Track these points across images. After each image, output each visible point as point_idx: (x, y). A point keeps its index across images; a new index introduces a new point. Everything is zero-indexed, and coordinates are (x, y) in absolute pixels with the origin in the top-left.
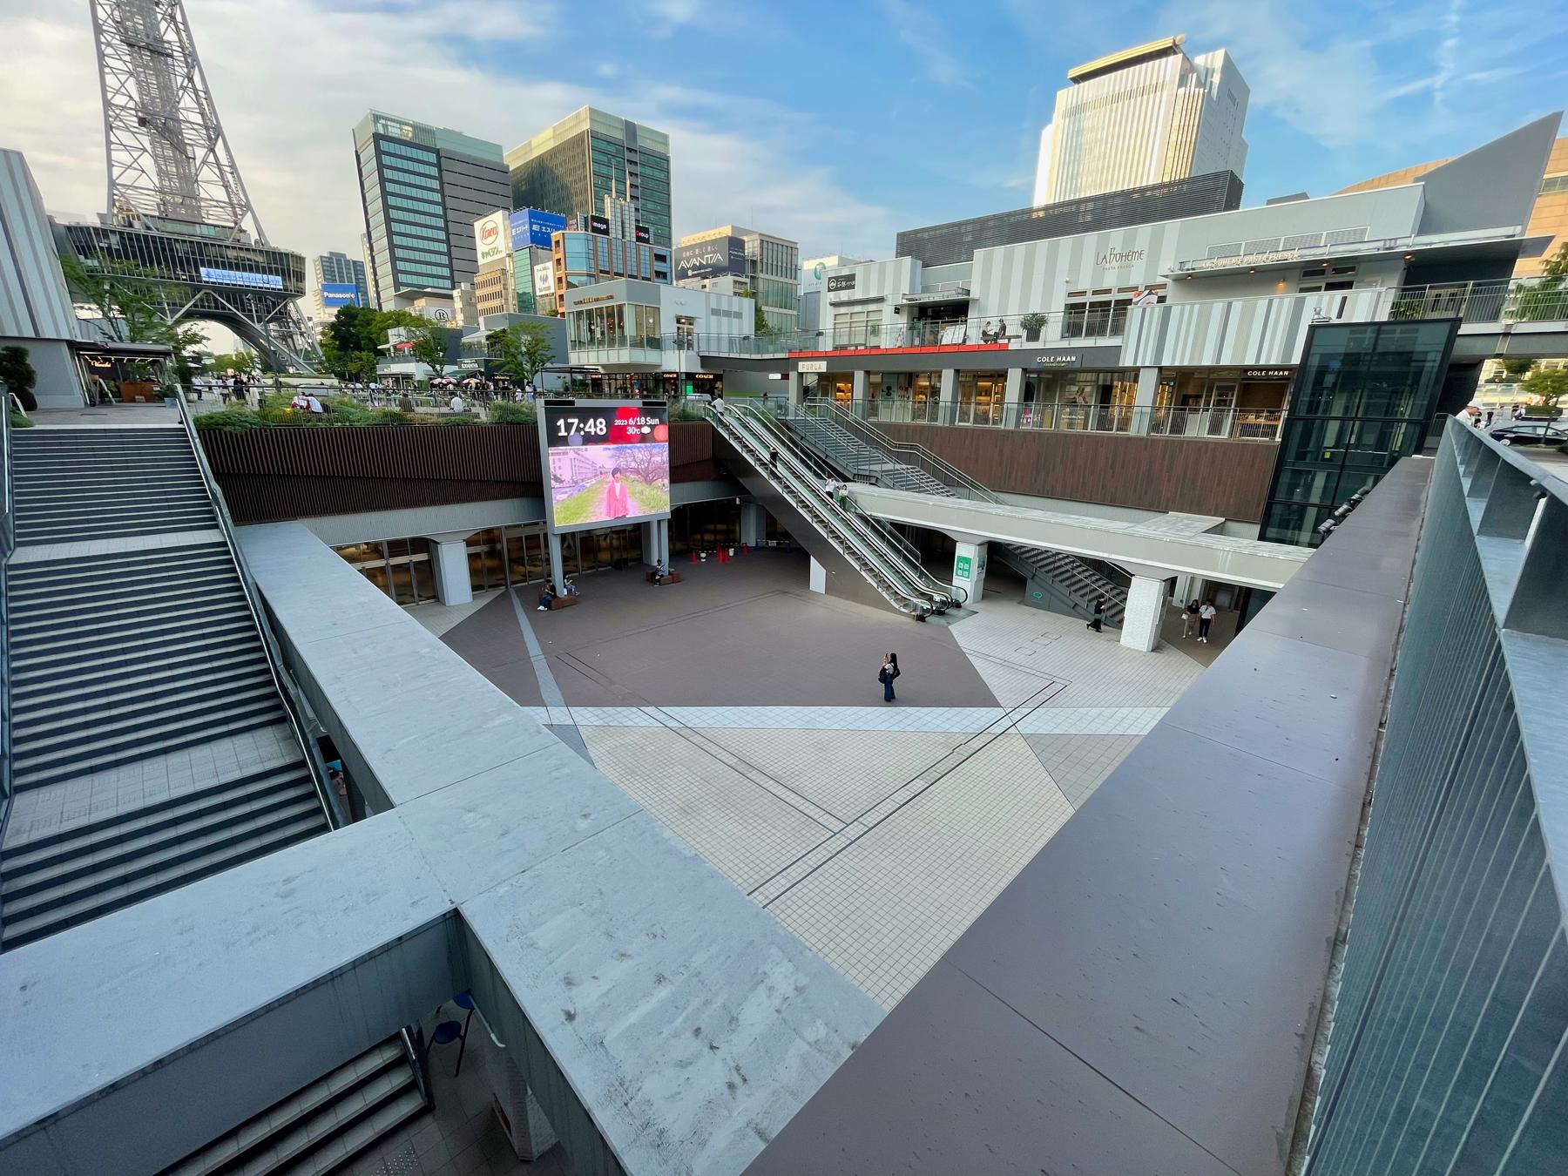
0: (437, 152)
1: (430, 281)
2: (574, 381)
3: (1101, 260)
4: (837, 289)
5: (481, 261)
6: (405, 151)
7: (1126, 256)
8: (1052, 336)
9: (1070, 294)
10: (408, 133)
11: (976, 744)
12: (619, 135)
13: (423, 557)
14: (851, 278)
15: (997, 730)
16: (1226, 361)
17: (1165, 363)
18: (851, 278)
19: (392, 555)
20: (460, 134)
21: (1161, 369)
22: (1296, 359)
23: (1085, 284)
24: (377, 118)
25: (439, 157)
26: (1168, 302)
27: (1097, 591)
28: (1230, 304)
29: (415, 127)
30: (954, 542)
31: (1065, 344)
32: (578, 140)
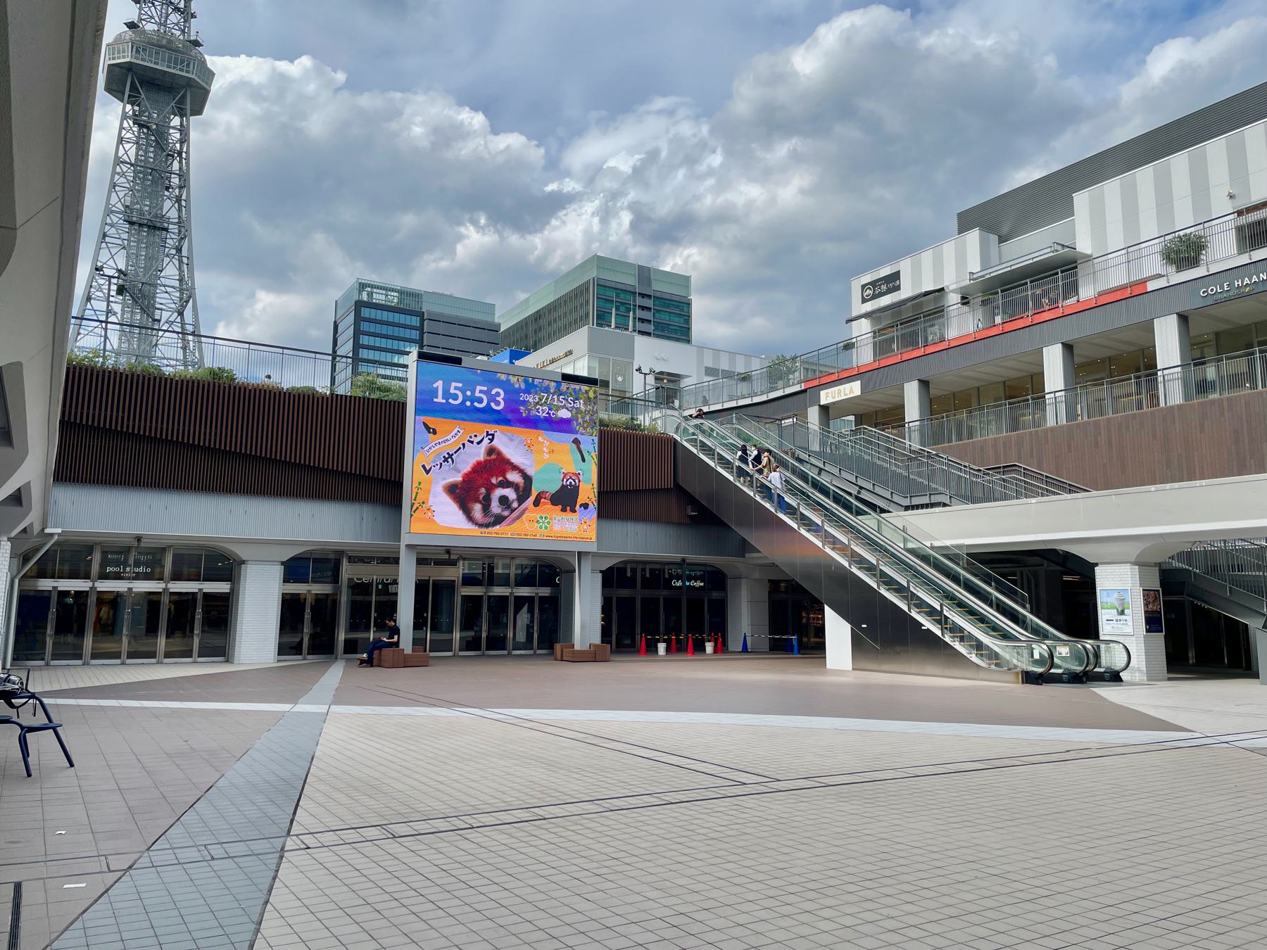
0: (421, 315)
4: (874, 297)
6: (385, 316)
8: (1224, 252)
10: (394, 299)
12: (630, 280)
14: (896, 276)
18: (896, 276)
19: (176, 577)
24: (362, 286)
25: (422, 320)
31: (1244, 259)
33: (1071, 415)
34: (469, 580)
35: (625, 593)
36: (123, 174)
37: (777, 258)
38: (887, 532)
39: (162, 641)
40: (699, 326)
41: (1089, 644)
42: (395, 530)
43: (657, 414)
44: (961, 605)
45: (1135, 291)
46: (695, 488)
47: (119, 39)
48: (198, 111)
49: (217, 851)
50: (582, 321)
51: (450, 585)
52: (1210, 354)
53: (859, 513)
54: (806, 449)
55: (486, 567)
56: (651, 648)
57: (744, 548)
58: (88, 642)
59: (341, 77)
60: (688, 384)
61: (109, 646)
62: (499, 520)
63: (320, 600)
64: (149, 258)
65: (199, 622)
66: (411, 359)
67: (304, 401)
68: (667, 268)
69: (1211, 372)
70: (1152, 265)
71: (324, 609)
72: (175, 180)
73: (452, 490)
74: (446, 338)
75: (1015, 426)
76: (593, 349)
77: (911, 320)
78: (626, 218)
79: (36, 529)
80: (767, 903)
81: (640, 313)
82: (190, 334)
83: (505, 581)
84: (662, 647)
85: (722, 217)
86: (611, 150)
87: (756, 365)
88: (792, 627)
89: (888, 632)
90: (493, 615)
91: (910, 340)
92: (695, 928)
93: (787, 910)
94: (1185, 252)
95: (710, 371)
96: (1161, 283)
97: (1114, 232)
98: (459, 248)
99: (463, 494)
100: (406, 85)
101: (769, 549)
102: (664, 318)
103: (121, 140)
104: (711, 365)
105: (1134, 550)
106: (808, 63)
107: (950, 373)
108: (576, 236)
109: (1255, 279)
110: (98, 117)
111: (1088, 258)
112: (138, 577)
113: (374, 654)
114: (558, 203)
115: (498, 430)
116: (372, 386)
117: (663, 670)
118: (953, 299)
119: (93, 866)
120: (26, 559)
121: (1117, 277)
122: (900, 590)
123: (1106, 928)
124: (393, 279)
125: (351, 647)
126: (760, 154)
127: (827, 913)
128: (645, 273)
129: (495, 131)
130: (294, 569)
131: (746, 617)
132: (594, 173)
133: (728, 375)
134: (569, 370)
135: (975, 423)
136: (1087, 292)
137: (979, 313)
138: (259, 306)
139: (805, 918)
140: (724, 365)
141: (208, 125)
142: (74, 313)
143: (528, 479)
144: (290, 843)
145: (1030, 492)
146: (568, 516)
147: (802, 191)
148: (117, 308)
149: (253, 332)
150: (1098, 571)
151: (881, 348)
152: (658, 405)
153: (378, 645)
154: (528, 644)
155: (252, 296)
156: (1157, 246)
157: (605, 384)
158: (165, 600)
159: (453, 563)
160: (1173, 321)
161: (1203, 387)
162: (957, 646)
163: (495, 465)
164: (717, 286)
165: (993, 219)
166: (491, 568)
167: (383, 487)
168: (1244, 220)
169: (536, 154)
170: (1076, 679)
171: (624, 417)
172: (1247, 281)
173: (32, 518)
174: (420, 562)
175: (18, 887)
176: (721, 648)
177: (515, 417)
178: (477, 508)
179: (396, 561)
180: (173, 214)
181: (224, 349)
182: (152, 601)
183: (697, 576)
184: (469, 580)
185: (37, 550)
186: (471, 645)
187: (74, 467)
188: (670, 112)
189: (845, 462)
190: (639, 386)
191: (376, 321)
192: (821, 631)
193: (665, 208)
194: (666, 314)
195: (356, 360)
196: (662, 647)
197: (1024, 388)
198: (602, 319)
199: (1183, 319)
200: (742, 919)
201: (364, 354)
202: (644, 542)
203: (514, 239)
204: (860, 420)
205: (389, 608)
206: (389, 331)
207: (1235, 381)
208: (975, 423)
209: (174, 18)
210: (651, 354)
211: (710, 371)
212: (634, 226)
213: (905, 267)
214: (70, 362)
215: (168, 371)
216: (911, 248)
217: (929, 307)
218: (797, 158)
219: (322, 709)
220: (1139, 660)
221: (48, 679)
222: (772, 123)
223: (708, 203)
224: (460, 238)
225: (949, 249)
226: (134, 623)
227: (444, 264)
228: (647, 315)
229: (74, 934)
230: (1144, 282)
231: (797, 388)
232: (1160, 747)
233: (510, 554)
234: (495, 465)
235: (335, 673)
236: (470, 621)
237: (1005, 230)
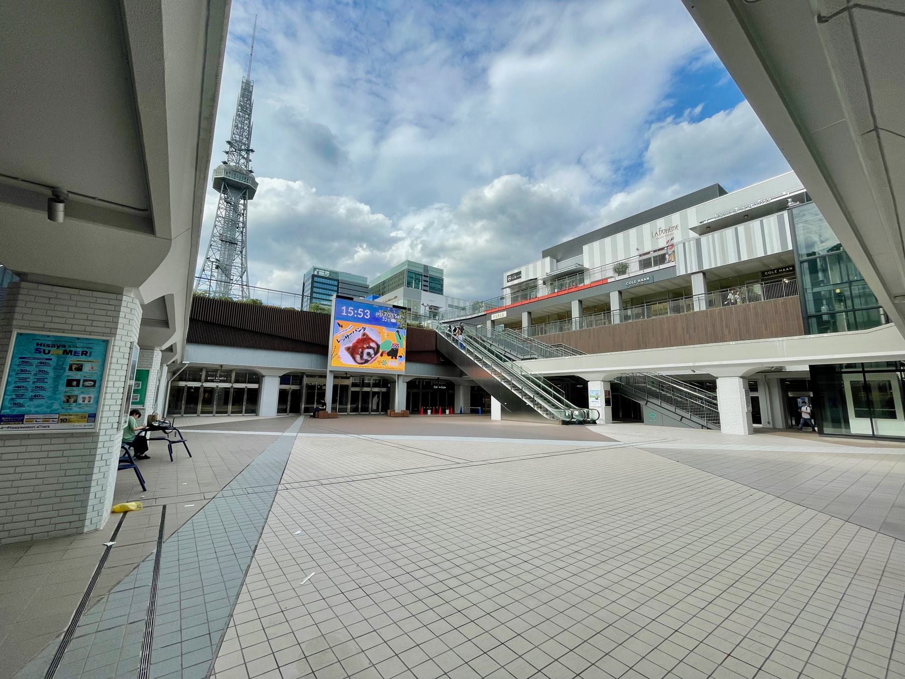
0: (338, 281)
3: (654, 235)
7: (669, 230)
8: (634, 269)
10: (327, 274)
12: (421, 271)
14: (520, 273)
16: (744, 258)
17: (706, 267)
18: (520, 273)
19: (237, 381)
20: (350, 274)
21: (704, 273)
22: (790, 248)
23: (648, 247)
24: (315, 269)
27: (695, 398)
28: (736, 229)
29: (330, 272)
30: (585, 383)
31: (641, 272)
32: (402, 273)
33: (581, 327)
34: (354, 385)
35: (415, 391)
36: (220, 221)
37: (479, 267)
38: (515, 368)
39: (230, 407)
40: (446, 289)
41: (585, 410)
42: (325, 364)
43: (429, 322)
44: (541, 396)
45: (604, 282)
46: (444, 351)
47: (219, 168)
48: (251, 198)
49: (250, 490)
50: (399, 286)
51: (347, 387)
52: (629, 306)
53: (505, 361)
54: (485, 337)
55: (361, 379)
56: (425, 412)
57: (462, 374)
58: (200, 407)
59: (314, 190)
60: (439, 313)
61: (208, 409)
62: (367, 361)
63: (294, 392)
64: (229, 255)
65: (245, 400)
66: (334, 298)
67: (290, 313)
68: (435, 266)
69: (629, 312)
70: (610, 273)
71: (296, 395)
72: (241, 225)
73: (348, 349)
74: (346, 290)
75: (561, 329)
76: (405, 295)
77: (525, 289)
78: (420, 246)
79: (179, 362)
80: (467, 508)
81: (424, 283)
82: (245, 285)
83: (368, 385)
84: (429, 411)
85: (456, 248)
86: (417, 221)
87: (468, 305)
88: (479, 404)
89: (515, 406)
90: (364, 398)
91: (525, 297)
92: (439, 518)
93: (474, 510)
94: (621, 269)
95: (450, 306)
96: (613, 280)
97: (598, 260)
98: (356, 256)
99: (352, 351)
100: (339, 195)
101: (471, 375)
102: (433, 285)
103: (219, 208)
105: (602, 376)
106: (491, 193)
107: (538, 310)
108: (402, 253)
110: (208, 197)
111: (588, 269)
112: (221, 381)
113: (315, 412)
114: (395, 240)
115: (367, 326)
116: (317, 308)
117: (429, 420)
118: (540, 282)
119: (198, 497)
120: (174, 373)
121: (598, 277)
122: (518, 389)
123: (590, 514)
124: (326, 267)
125: (307, 410)
126: (471, 225)
127: (489, 511)
128: (426, 268)
129: (373, 213)
130: (284, 379)
131: (462, 401)
132: (410, 231)
133: (457, 307)
134: (396, 304)
135: (547, 328)
136: (587, 282)
137: (549, 288)
138: (274, 276)
139: (481, 513)
140: (456, 304)
141: (256, 205)
142: (197, 275)
143: (378, 346)
144: (280, 488)
145: (567, 354)
146: (394, 360)
147: (487, 241)
148: (215, 274)
149: (271, 286)
151: (514, 299)
152: (430, 318)
153: (318, 410)
154: (377, 410)
155: (272, 272)
156: (611, 267)
157: (410, 310)
158: (232, 391)
159: (348, 378)
161: (627, 318)
162: (539, 411)
163: (366, 339)
164: (453, 274)
165: (555, 253)
166: (363, 380)
167: (321, 348)
168: (642, 258)
169: (388, 222)
170: (581, 423)
171: (417, 323)
173: (177, 357)
174: (335, 377)
175: (164, 507)
176: (452, 412)
177: (375, 321)
178: (358, 357)
179: (325, 377)
180: (240, 238)
181: (260, 292)
182: (226, 391)
183: (443, 383)
184: (354, 385)
185: (179, 370)
186: (355, 410)
187: (193, 338)
188: (441, 209)
189: (500, 342)
190: (423, 311)
191: (319, 283)
192: (489, 406)
193: (435, 243)
194: (434, 284)
195: (312, 297)
196: (429, 411)
197: (564, 316)
198: (409, 284)
199: (620, 292)
200: (457, 514)
201: (315, 295)
202: (422, 371)
203: (377, 253)
204: (506, 326)
205: (322, 395)
206: (326, 286)
207: (637, 316)
208: (547, 328)
209: (242, 161)
210: (428, 299)
211: (450, 306)
212: (422, 249)
213: (523, 269)
214: (194, 295)
215: (235, 300)
216: (526, 263)
217: (531, 285)
218: (484, 228)
219: (295, 434)
220: (602, 416)
221: (181, 422)
222: (476, 214)
223: (451, 242)
224: (357, 252)
225: (539, 263)
226: (219, 399)
227: (349, 262)
228: (427, 284)
229: (188, 526)
230: (607, 279)
232: (609, 448)
233: (371, 375)
234: (366, 339)
235: (300, 420)
236: (354, 400)
237: (559, 258)
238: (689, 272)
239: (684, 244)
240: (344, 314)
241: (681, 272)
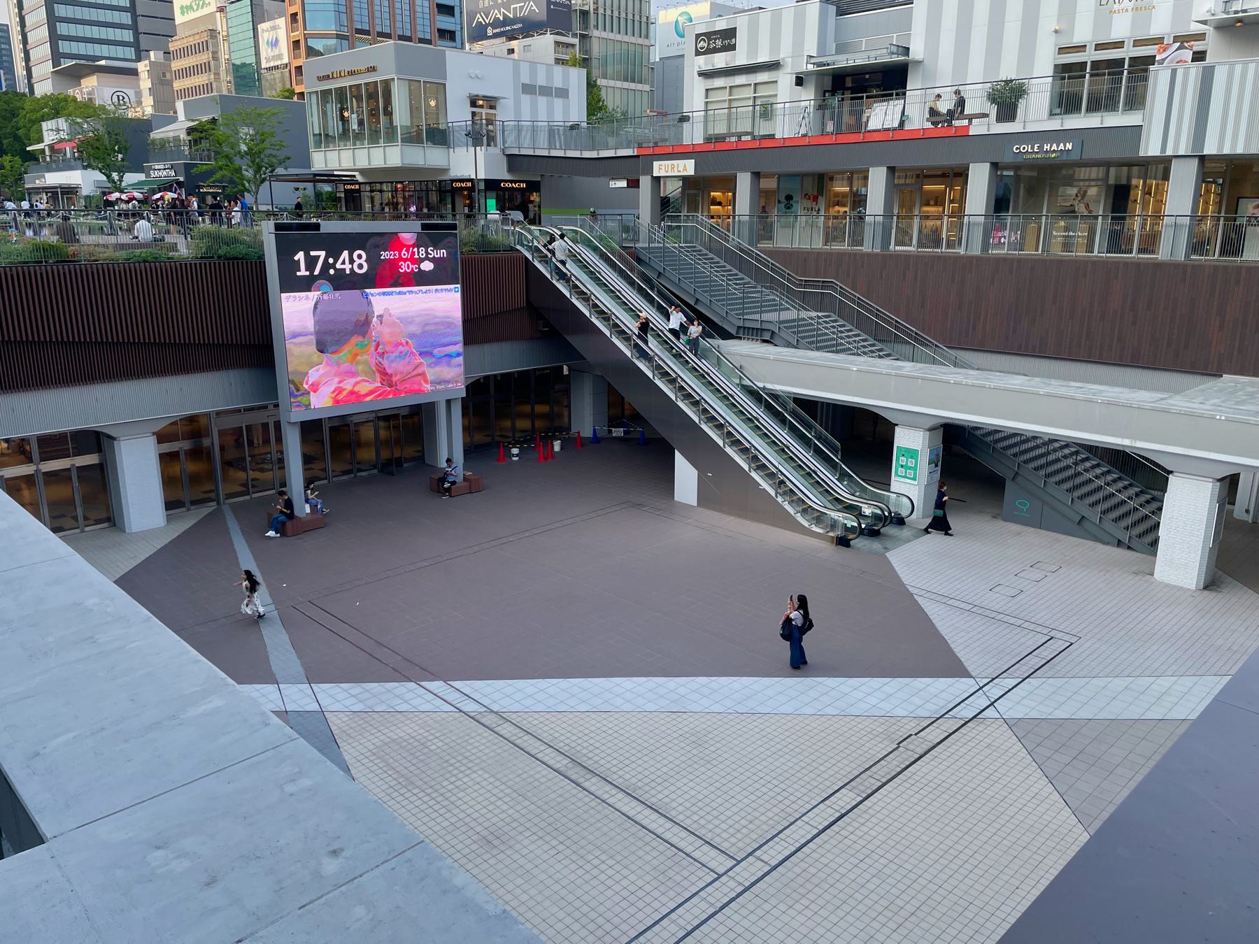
1: (104, 50)
2: (318, 195)
5: (179, 19)
8: (1036, 113)
9: (1062, 50)
11: (934, 735)
13: (90, 459)
14: (730, 33)
15: (967, 712)
17: (1210, 149)
18: (730, 33)
19: (45, 457)
21: (1202, 159)
23: (1083, 33)
26: (1209, 59)
30: (889, 427)
31: (1055, 124)
94: (1007, 99)
104: (527, 81)
109: (1062, 147)
150: (899, 431)
160: (986, 167)
167: (256, 348)
172: (1054, 147)
231: (629, 152)
238: (1169, 152)
239: (1174, 72)
240: (303, 272)
241: (1151, 148)
